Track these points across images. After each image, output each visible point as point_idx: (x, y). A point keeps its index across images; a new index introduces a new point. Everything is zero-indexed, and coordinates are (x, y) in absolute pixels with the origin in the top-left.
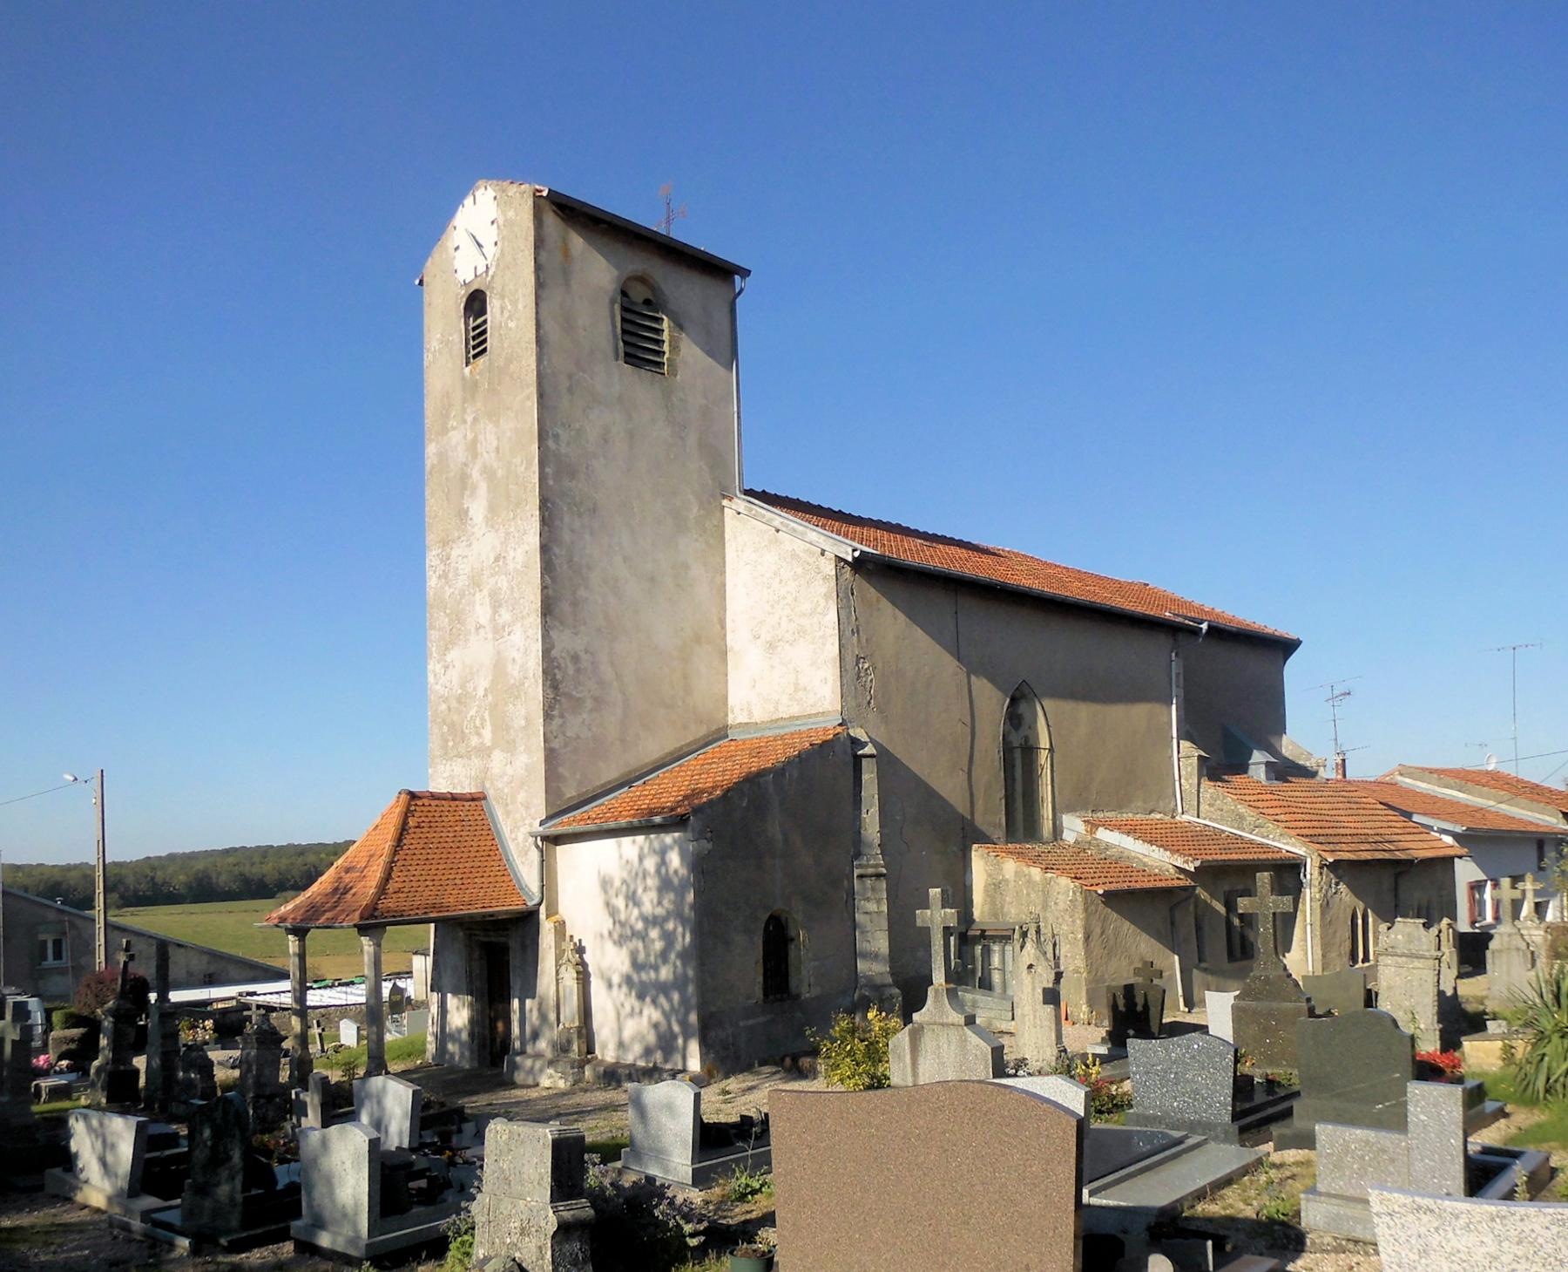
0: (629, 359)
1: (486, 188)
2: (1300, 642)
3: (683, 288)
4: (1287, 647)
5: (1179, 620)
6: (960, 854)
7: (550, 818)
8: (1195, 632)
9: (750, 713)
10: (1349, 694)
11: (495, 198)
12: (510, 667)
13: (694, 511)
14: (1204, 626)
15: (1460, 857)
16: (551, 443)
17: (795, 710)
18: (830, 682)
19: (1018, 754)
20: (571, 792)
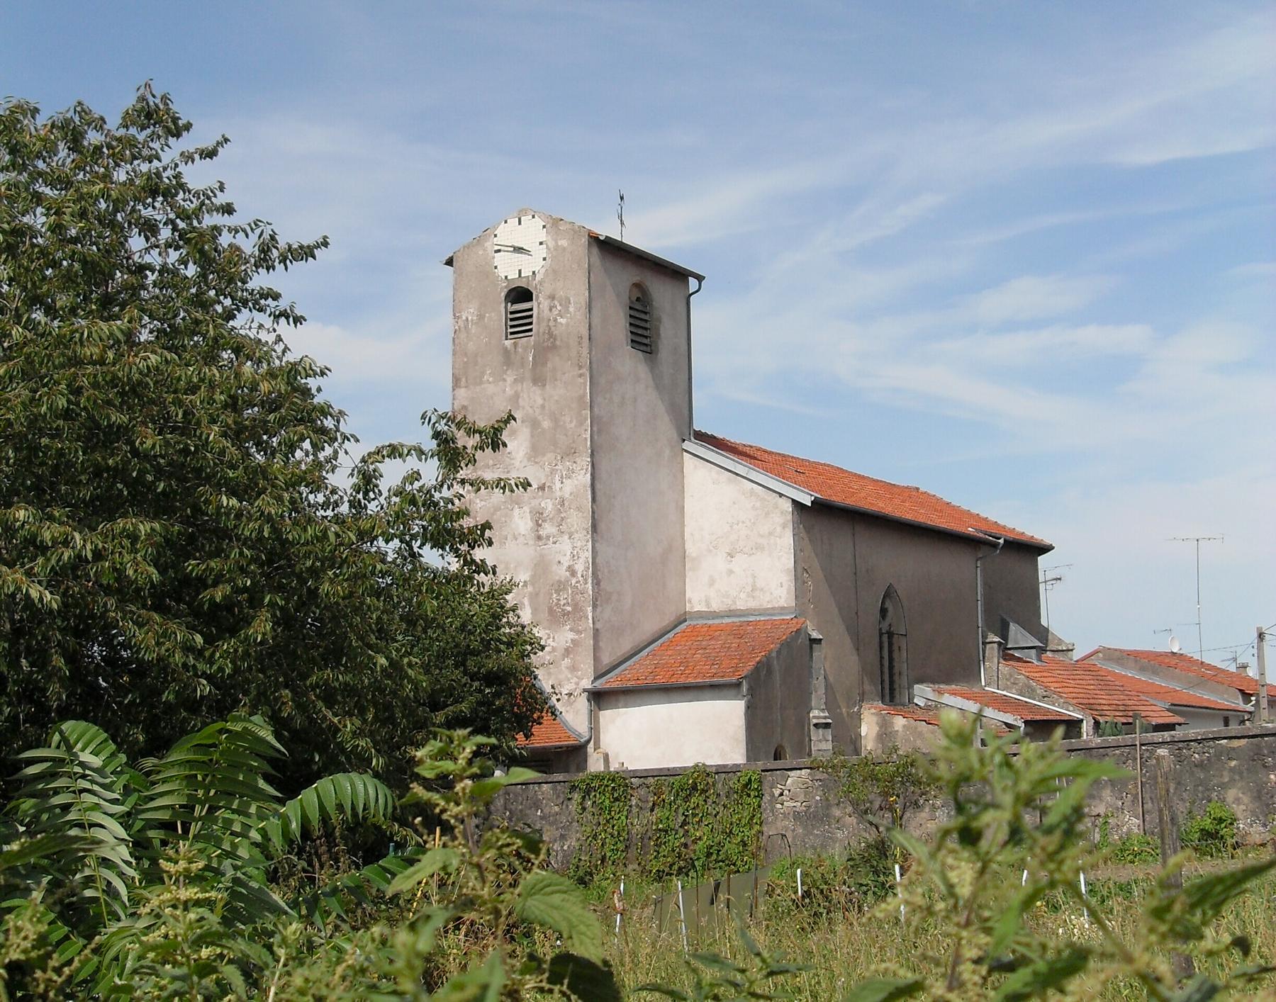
0: (635, 345)
1: (533, 217)
2: (1053, 548)
3: (661, 292)
4: (1044, 549)
5: (981, 535)
6: (15, 912)
7: (596, 679)
8: (994, 546)
9: (708, 605)
10: (1060, 579)
11: (544, 227)
12: (555, 567)
13: (667, 452)
14: (1001, 541)
15: (1180, 724)
16: (596, 410)
17: (752, 604)
18: (786, 586)
19: (885, 638)
20: (607, 660)
